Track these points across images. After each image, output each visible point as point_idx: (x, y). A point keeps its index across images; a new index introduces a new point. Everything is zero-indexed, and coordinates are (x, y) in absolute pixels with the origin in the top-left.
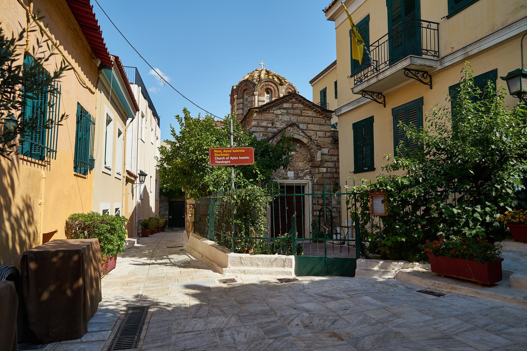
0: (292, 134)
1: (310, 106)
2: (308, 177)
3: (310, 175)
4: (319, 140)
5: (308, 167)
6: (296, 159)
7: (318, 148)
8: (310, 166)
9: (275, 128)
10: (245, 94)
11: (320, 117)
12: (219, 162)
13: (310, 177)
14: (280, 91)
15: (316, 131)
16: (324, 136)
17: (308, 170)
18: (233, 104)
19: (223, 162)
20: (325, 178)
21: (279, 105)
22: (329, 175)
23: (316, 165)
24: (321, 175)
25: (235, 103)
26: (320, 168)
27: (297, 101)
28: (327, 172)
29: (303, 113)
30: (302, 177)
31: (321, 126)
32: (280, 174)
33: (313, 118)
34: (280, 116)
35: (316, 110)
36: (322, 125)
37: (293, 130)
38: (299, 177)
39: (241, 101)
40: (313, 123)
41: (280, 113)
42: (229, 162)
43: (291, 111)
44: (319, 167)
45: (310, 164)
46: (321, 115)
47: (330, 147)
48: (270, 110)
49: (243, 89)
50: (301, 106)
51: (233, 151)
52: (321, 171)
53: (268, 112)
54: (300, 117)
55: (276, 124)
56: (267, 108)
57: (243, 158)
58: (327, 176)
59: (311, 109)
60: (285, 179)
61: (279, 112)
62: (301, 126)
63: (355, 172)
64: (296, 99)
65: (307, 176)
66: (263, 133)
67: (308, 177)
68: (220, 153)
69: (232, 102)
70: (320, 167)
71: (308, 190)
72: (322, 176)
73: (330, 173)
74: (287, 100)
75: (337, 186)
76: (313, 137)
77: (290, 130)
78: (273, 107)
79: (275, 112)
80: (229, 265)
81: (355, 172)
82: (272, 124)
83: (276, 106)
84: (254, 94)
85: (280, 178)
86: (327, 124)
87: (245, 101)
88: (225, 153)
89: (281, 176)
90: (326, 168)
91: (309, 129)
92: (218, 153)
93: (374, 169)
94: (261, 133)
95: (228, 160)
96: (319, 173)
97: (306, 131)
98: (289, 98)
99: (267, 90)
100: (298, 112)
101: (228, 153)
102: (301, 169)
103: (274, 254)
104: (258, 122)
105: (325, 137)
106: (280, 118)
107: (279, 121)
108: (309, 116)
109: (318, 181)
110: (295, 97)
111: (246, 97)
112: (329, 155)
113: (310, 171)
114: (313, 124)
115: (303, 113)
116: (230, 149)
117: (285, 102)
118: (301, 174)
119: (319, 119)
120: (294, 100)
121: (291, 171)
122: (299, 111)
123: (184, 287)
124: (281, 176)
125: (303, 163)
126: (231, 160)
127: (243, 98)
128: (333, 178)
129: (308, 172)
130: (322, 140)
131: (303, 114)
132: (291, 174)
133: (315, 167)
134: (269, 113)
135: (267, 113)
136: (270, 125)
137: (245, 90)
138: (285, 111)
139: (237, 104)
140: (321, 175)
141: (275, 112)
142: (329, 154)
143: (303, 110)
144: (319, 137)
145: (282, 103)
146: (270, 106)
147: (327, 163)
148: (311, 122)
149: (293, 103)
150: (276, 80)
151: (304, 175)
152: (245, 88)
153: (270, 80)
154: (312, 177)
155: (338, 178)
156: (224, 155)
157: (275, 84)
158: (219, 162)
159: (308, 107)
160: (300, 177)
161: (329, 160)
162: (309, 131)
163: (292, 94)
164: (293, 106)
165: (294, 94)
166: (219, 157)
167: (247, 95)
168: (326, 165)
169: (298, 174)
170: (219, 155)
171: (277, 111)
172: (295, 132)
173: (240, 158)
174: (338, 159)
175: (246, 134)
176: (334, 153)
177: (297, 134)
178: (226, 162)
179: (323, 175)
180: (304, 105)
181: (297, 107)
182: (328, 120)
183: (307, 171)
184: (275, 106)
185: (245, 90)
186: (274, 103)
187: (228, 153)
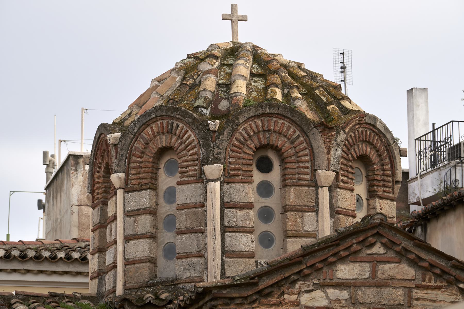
1: (443, 272)
10: (162, 166)
14: (322, 159)
18: (105, 204)
21: (319, 270)
27: (391, 254)
29: (418, 299)
48: (283, 293)
49: (153, 148)
53: (275, 300)
56: (272, 286)
59: (450, 283)
74: (352, 249)
78: (294, 282)
83: (308, 275)
84: (202, 172)
87: (161, 201)
98: (358, 243)
99: (261, 153)
110: (382, 236)
115: (418, 299)
117: (342, 260)
120: (378, 249)
122: (400, 292)
127: (154, 188)
134: (280, 304)
135: (272, 305)
137: (163, 151)
138: (344, 295)
139: (127, 214)
143: (418, 287)
145: (333, 264)
146: (286, 279)
152: (163, 141)
153: (275, 111)
159: (435, 274)
163: (373, 228)
164: (374, 272)
165: (380, 225)
167: (170, 172)
171: (313, 294)
175: (70, 185)
180: (421, 267)
181: (392, 279)
184: (305, 277)
185: (163, 151)
186: (300, 263)
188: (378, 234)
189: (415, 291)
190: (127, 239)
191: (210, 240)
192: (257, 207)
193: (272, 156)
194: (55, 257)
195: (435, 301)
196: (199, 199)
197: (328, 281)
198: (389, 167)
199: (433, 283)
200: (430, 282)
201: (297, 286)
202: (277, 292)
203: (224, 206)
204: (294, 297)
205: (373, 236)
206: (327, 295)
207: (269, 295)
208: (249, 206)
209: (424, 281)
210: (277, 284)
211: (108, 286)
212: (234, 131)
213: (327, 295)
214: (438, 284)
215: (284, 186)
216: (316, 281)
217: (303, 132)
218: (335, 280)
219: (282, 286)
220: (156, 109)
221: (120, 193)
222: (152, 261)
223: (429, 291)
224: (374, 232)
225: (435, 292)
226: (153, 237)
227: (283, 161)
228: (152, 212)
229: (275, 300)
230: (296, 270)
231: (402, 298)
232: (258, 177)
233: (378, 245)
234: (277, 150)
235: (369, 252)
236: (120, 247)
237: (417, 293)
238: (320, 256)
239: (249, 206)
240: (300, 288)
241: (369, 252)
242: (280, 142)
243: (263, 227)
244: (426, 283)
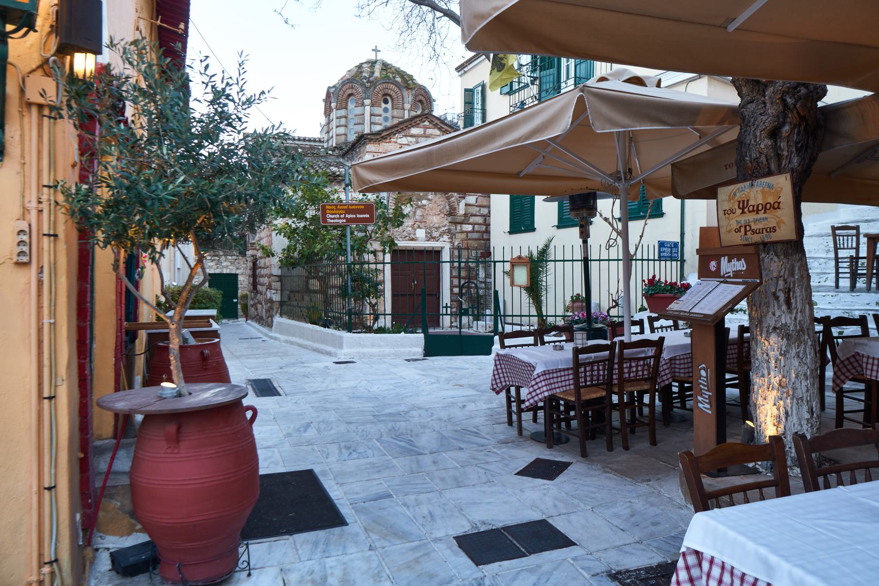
2: (446, 238)
5: (446, 222)
8: (450, 222)
12: (332, 221)
14: (406, 100)
17: (446, 228)
19: (336, 221)
20: (470, 239)
22: (476, 235)
23: (458, 220)
24: (464, 236)
25: (333, 115)
26: (464, 225)
27: (431, 125)
28: (473, 231)
32: (405, 233)
38: (434, 238)
39: (343, 112)
41: (406, 143)
42: (345, 221)
44: (461, 223)
45: (450, 219)
51: (350, 207)
52: (464, 229)
57: (361, 216)
60: (413, 240)
61: (404, 141)
63: (511, 233)
64: (431, 122)
67: (446, 238)
68: (333, 209)
69: (328, 112)
71: (446, 256)
73: (477, 232)
75: (487, 253)
78: (395, 134)
79: (399, 141)
80: (344, 346)
81: (511, 233)
84: (363, 103)
88: (339, 210)
92: (331, 210)
93: (534, 230)
95: (343, 218)
96: (462, 232)
101: (342, 209)
102: (437, 225)
103: (400, 333)
111: (351, 106)
112: (477, 206)
113: (449, 230)
116: (346, 205)
117: (413, 126)
120: (427, 123)
121: (421, 228)
123: (646, 82)
125: (438, 217)
126: (347, 219)
132: (421, 233)
133: (456, 223)
134: (390, 142)
137: (350, 95)
139: (337, 118)
140: (464, 236)
141: (399, 141)
145: (410, 128)
147: (473, 218)
149: (426, 128)
150: (399, 79)
151: (440, 235)
152: (349, 91)
154: (451, 238)
155: (489, 240)
156: (337, 212)
157: (396, 84)
158: (332, 221)
160: (434, 238)
161: (478, 214)
164: (425, 132)
166: (332, 214)
167: (352, 103)
168: (472, 220)
169: (431, 233)
170: (332, 212)
173: (358, 216)
174: (489, 212)
176: (485, 203)
178: (341, 221)
179: (474, 227)
183: (444, 229)
185: (350, 95)
186: (397, 127)
187: (342, 209)
188: (427, 118)
190: (337, 127)
191: (366, 127)
192: (383, 116)
193: (389, 98)
194: (553, 423)
196: (362, 112)
198: (649, 360)
202: (389, 138)
203: (371, 115)
204: (395, 140)
207: (386, 138)
208: (380, 115)
210: (388, 135)
211: (330, 144)
212: (375, 88)
215: (393, 109)
217: (400, 90)
220: (347, 79)
221: (334, 110)
222: (346, 135)
226: (346, 126)
227: (392, 100)
228: (346, 117)
229: (388, 141)
232: (383, 105)
234: (390, 96)
236: (334, 130)
238: (405, 124)
239: (380, 115)
242: (391, 93)
243: (384, 115)
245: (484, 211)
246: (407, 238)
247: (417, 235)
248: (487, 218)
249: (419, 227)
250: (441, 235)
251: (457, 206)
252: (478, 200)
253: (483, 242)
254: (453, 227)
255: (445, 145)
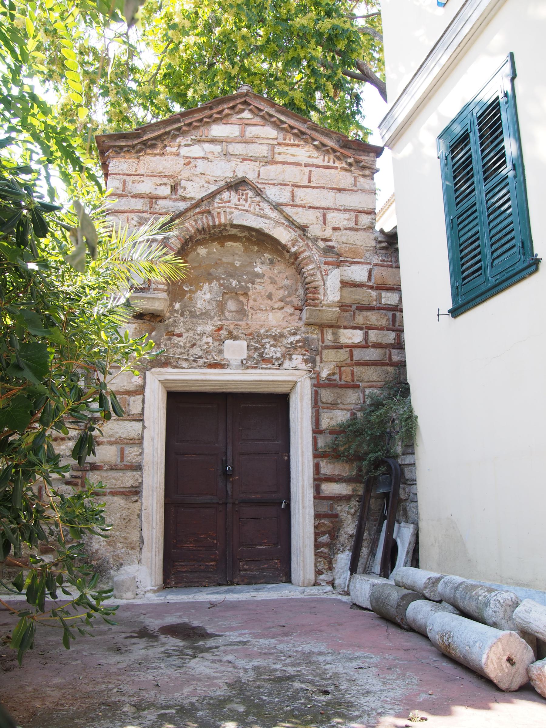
0: (236, 212)
3: (304, 355)
4: (334, 238)
6: (255, 300)
7: (329, 259)
8: (308, 324)
9: (184, 199)
11: (336, 168)
13: (306, 361)
15: (323, 208)
16: (352, 224)
17: (297, 338)
22: (373, 354)
24: (343, 354)
26: (342, 331)
27: (257, 120)
28: (365, 345)
29: (279, 154)
30: (277, 359)
31: (338, 195)
33: (313, 169)
34: (200, 163)
35: (324, 145)
36: (344, 190)
37: (239, 200)
38: (269, 361)
40: (312, 184)
41: (202, 154)
43: (238, 149)
46: (339, 158)
47: (376, 261)
48: (166, 146)
50: (270, 132)
54: (269, 167)
55: (185, 189)
56: (155, 138)
58: (368, 358)
61: (196, 151)
62: (272, 193)
65: (294, 357)
66: (140, 214)
67: (298, 360)
70: (340, 327)
72: (347, 355)
73: (376, 346)
76: (315, 230)
77: (229, 202)
78: (175, 137)
82: (174, 188)
85: (194, 364)
86: (359, 187)
89: (200, 357)
90: (360, 328)
91: (298, 202)
94: (131, 215)
97: (288, 210)
100: (262, 150)
102: (276, 331)
104: (124, 182)
105: (357, 230)
106: (199, 170)
107: (197, 179)
108: (299, 165)
109: (334, 374)
112: (371, 288)
114: (313, 188)
115: (279, 154)
118: (273, 349)
119: (332, 171)
121: (236, 338)
122: (265, 147)
124: (200, 357)
125: (279, 315)
128: (387, 365)
129: (298, 341)
130: (344, 239)
131: (278, 158)
135: (156, 155)
136: (166, 191)
138: (217, 148)
141: (184, 151)
142: (370, 284)
143: (279, 144)
144: (335, 229)
147: (365, 313)
148: (306, 183)
154: (313, 361)
160: (269, 361)
162: (300, 209)
172: (246, 208)
174: (400, 300)
177: (253, 214)
179: (366, 334)
182: (364, 176)
189: (277, 147)
195: (294, 155)
197: (203, 137)
199: (292, 142)
200: (290, 141)
201: (178, 140)
202: (160, 145)
204: (174, 149)
205: (241, 103)
206: (203, 149)
207: (153, 146)
209: (285, 140)
213: (203, 149)
214: (297, 142)
216: (193, 137)
218: (210, 137)
219: (164, 140)
223: (289, 148)
224: (243, 100)
225: (295, 148)
229: (157, 151)
230: (176, 126)
231: (266, 152)
233: (247, 112)
235: (239, 117)
237: (278, 149)
240: (180, 142)
241: (239, 117)
244: (287, 141)
245: (389, 298)
246: (202, 361)
247: (227, 355)
248: (398, 314)
249: (231, 336)
250: (288, 355)
251: (321, 283)
252: (374, 273)
253: (390, 369)
254: (315, 336)
255: (380, 543)
